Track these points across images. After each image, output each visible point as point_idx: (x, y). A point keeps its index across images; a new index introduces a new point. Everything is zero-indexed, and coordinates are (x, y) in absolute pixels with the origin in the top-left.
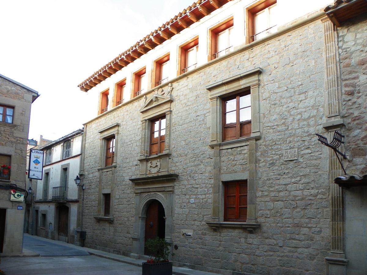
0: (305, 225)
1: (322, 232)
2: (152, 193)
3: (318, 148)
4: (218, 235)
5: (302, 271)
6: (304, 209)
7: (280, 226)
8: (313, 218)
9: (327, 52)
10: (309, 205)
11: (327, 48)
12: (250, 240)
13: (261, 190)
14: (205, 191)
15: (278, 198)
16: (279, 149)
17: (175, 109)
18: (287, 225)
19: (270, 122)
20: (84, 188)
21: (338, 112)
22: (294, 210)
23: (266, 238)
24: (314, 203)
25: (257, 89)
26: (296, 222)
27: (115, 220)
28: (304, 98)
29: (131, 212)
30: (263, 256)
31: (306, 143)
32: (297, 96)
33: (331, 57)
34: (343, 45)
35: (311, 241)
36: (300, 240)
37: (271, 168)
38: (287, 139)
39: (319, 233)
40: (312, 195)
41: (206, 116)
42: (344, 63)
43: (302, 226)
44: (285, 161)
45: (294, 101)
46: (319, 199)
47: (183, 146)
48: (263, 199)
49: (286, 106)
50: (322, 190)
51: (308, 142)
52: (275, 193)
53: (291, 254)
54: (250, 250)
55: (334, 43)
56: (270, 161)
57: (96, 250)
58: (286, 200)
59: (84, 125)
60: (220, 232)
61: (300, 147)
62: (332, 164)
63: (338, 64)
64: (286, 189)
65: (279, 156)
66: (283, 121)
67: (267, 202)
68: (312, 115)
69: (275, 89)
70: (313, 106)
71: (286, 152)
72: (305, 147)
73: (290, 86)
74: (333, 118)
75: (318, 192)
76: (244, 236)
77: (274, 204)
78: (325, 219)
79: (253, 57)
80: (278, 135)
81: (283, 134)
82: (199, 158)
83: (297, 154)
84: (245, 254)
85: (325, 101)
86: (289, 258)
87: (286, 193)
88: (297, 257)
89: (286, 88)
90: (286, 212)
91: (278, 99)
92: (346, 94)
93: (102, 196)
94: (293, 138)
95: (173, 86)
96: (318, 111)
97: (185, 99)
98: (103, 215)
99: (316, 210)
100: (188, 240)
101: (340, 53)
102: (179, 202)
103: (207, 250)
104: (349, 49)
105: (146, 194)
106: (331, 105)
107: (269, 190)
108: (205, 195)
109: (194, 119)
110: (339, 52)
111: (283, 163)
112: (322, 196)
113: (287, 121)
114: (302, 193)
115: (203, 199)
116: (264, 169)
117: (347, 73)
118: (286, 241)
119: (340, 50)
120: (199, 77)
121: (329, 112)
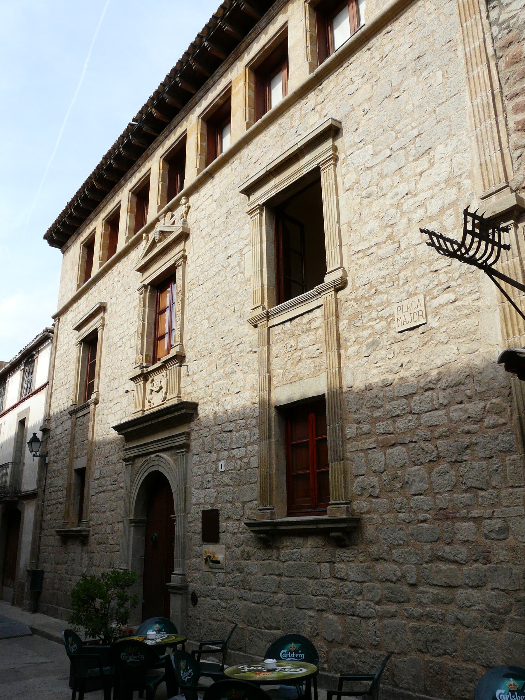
0: (464, 512)
1: (510, 532)
2: (152, 456)
3: (469, 285)
4: (274, 557)
5: (474, 671)
6: (456, 461)
7: (404, 521)
8: (481, 489)
9: (466, 41)
10: (467, 447)
11: (465, 32)
12: (341, 568)
13: (354, 420)
14: (246, 437)
15: (392, 436)
16: (385, 303)
17: (192, 252)
18: (420, 517)
19: (363, 239)
20: (47, 462)
21: (503, 180)
22: (432, 469)
23: (376, 560)
24: (479, 440)
25: (333, 169)
26: (441, 505)
27: (91, 533)
28: (427, 165)
29: (118, 510)
30: (374, 618)
31: (443, 277)
32: (412, 163)
33: (475, 50)
34: (499, 15)
35: (486, 564)
36: (456, 562)
37: (371, 357)
38: (400, 275)
39: (502, 536)
40: (471, 420)
41: (243, 253)
42: (506, 57)
43: (458, 515)
44: (400, 332)
45: (406, 177)
46: (490, 427)
47: (205, 333)
48: (360, 445)
49: (392, 193)
50: (494, 400)
51: (446, 272)
52: (385, 423)
53: (439, 610)
54: (343, 598)
55: (478, 16)
56: (368, 338)
57: (57, 620)
58: (412, 442)
59: (54, 317)
60: (278, 549)
61: (428, 288)
62: (506, 322)
63: (492, 64)
64: (409, 409)
65: (387, 322)
66: (389, 230)
67: (370, 452)
68: (447, 202)
69: (366, 159)
70: (447, 181)
71: (399, 308)
72: (440, 287)
73: (395, 146)
74: (494, 196)
75: (485, 406)
76: (327, 556)
77: (385, 454)
78: (511, 490)
79: (322, 100)
80: (380, 270)
81: (391, 263)
82: (233, 355)
83: (423, 309)
84: (335, 613)
85: (472, 159)
86: (436, 622)
87: (410, 421)
88: (458, 619)
89: (389, 150)
90: (415, 476)
91: (375, 181)
92: (518, 130)
93: (73, 474)
94: (411, 268)
95: (190, 203)
96: (459, 189)
97: (207, 225)
98: (73, 523)
99: (484, 464)
100: (217, 574)
101: (495, 34)
102: (199, 473)
103: (253, 605)
104: (515, 19)
105: (143, 460)
106: (486, 165)
107: (372, 417)
108: (246, 448)
109: (223, 266)
110: (492, 34)
111: (395, 338)
112: (496, 417)
113: (396, 228)
114: (447, 414)
115: (241, 459)
116: (357, 363)
117: (515, 78)
118: (425, 565)
119: (495, 29)
120: (232, 170)
121: (484, 186)
